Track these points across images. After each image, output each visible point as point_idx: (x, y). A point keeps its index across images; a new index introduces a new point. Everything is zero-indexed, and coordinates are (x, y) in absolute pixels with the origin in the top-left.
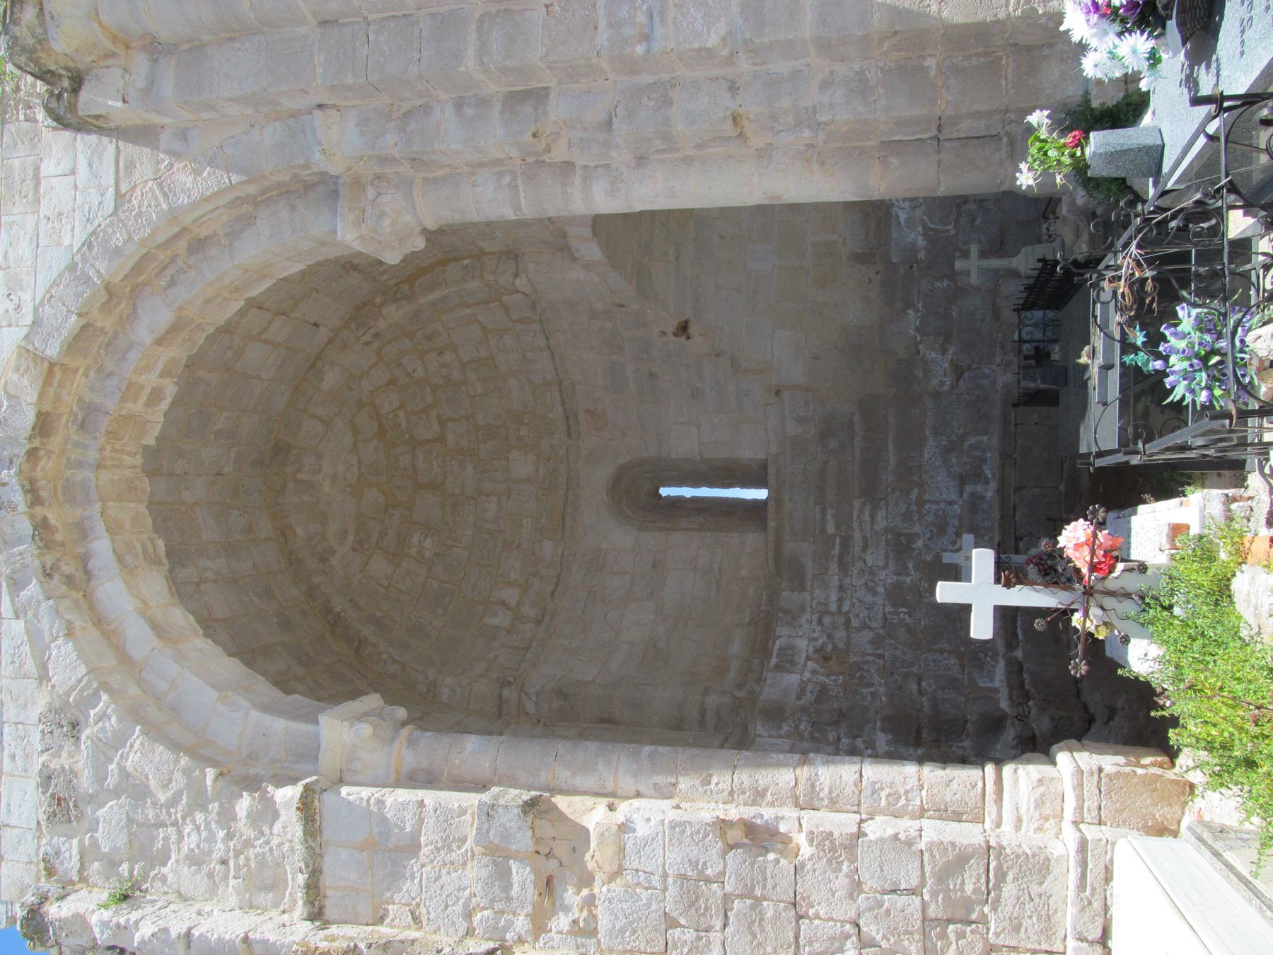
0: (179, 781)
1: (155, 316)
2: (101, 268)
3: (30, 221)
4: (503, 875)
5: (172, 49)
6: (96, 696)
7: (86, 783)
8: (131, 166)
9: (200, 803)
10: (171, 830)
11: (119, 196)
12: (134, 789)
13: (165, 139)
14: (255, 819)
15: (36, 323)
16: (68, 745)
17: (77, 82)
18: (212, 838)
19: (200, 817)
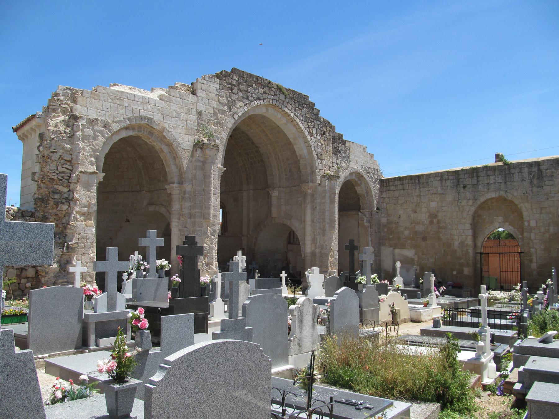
0: (97, 147)
1: (165, 149)
2: (175, 144)
3: (183, 133)
4: (85, 207)
5: (204, 165)
6: (110, 132)
7: (96, 128)
8: (188, 152)
9: (94, 151)
10: (88, 144)
11: (184, 149)
12: (95, 138)
13: (191, 159)
14: (91, 161)
15: (169, 131)
16: (102, 125)
17: (201, 148)
18: (87, 152)
19: (91, 150)
